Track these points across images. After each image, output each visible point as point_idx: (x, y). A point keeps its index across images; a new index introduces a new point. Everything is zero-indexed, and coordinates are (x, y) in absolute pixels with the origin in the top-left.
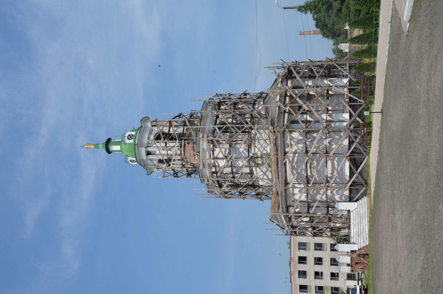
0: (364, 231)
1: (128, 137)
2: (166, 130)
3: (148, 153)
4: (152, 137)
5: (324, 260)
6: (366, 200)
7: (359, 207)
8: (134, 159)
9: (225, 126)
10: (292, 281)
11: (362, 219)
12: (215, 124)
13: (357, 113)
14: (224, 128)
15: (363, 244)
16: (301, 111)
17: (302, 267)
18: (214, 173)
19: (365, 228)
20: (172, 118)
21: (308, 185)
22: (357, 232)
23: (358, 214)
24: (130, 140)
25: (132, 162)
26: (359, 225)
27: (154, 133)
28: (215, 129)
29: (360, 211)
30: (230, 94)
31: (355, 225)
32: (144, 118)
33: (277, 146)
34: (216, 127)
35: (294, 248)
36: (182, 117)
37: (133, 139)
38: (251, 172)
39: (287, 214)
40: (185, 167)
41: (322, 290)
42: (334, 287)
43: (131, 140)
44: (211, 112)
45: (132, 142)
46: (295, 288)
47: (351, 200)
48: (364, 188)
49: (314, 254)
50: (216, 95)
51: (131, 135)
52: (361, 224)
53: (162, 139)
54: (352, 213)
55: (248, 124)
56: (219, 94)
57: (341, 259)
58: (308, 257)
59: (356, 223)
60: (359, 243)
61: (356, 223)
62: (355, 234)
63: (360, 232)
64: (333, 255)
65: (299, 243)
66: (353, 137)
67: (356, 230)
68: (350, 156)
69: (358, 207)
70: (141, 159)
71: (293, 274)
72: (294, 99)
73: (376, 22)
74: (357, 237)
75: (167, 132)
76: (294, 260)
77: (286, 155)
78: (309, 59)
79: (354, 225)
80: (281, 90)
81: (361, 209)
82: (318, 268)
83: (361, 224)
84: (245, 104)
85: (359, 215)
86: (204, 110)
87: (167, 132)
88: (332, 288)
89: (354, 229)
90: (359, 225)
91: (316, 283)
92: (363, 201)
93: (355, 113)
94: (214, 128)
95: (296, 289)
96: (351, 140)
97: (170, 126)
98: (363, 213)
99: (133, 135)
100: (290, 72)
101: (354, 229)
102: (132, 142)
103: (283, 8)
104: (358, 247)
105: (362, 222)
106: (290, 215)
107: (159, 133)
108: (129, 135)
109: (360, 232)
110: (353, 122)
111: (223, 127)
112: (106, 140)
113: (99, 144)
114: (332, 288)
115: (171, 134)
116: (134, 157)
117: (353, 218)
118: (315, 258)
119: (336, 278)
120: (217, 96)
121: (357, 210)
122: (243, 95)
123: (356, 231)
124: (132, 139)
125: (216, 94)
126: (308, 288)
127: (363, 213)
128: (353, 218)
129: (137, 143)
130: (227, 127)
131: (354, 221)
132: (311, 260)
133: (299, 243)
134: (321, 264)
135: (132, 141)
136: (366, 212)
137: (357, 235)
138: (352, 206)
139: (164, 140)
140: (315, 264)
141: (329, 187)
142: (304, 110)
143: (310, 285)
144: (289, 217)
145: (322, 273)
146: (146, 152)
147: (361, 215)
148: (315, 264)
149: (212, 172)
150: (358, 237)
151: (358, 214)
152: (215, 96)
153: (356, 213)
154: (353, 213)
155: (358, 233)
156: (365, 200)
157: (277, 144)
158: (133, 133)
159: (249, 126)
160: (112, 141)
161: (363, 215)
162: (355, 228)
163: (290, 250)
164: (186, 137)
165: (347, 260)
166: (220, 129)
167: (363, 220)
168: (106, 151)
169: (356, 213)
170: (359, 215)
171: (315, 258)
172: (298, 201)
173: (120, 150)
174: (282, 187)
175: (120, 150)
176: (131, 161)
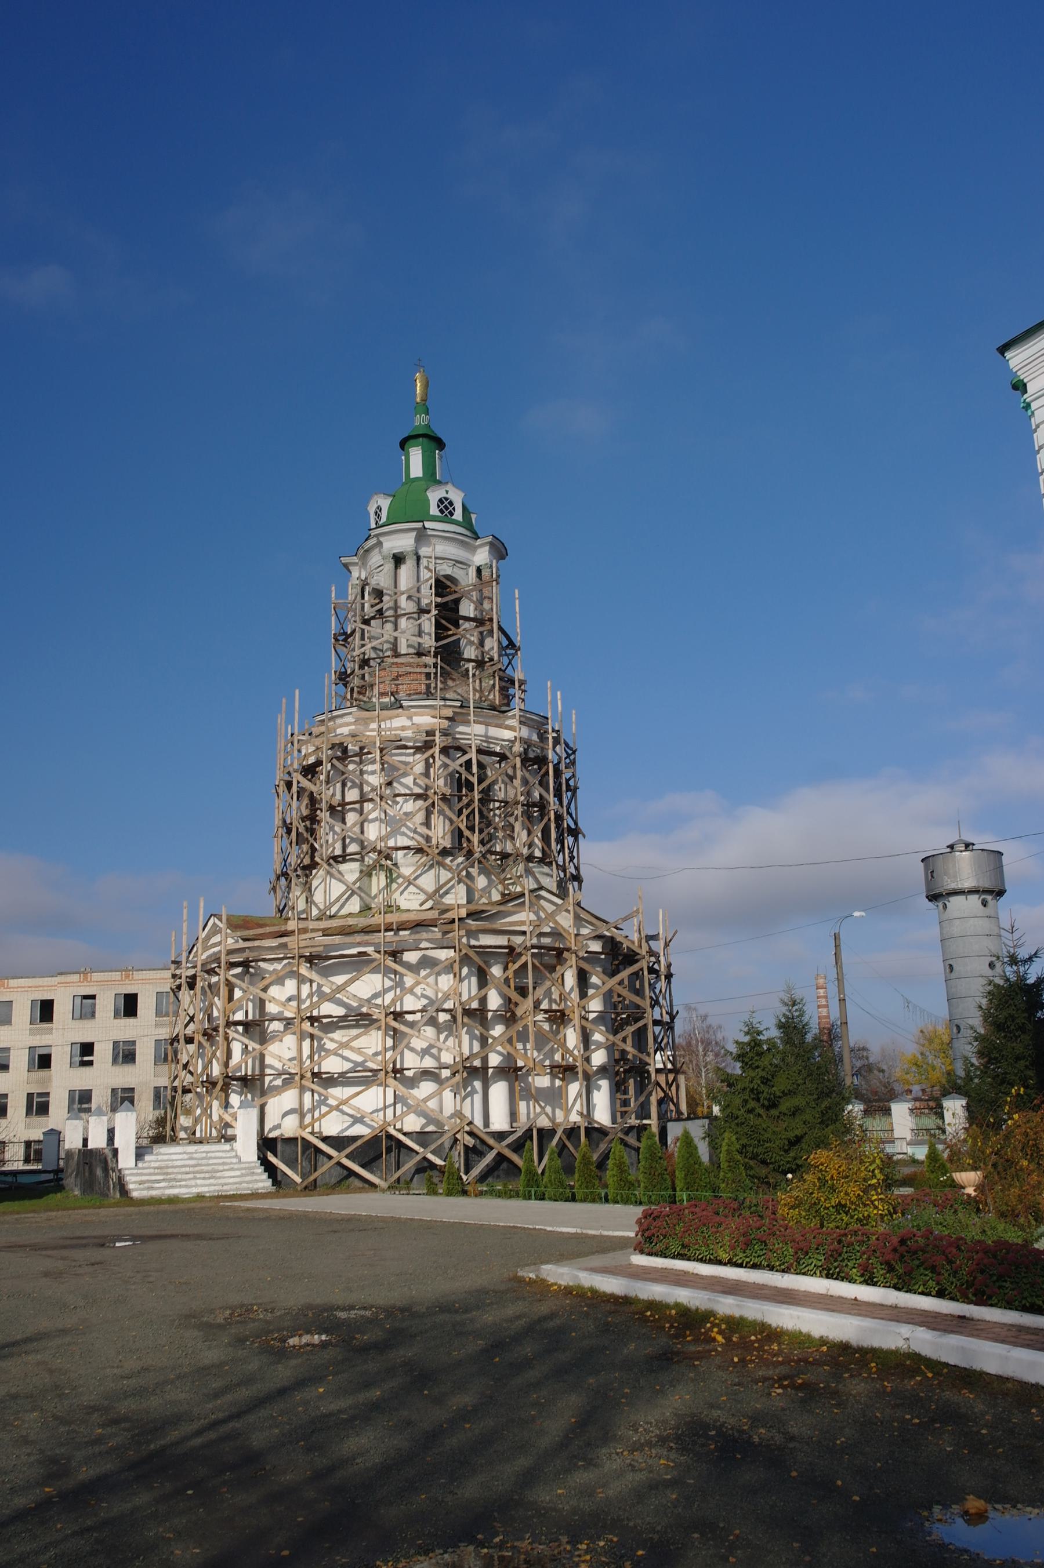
0: (171, 1184)
1: (446, 499)
2: (467, 609)
3: (398, 560)
4: (446, 569)
5: (128, 1068)
6: (261, 1185)
7: (243, 1166)
8: (384, 519)
9: (475, 780)
10: (63, 976)
11: (207, 1175)
12: (480, 751)
13: (508, 1153)
14: (470, 778)
15: (135, 1182)
16: (515, 996)
17: (106, 1005)
18: (345, 750)
19: (180, 1187)
20: (502, 626)
21: (392, 1016)
22: (170, 1164)
23: (224, 1164)
24: (439, 506)
25: (376, 513)
26: (192, 1169)
27: (457, 573)
28: (465, 753)
29: (232, 1169)
30: (576, 788)
31: (191, 1159)
32: (503, 544)
33: (415, 929)
34: (473, 755)
35: (163, 979)
36: (507, 655)
37: (440, 514)
38: (348, 858)
39: (223, 964)
40: (361, 667)
41: (39, 1068)
42: (48, 1101)
43: (437, 510)
44: (515, 737)
45: (431, 513)
46: (43, 986)
47: (267, 1144)
48: (298, 1179)
49: (145, 1039)
50: (571, 749)
51: (454, 509)
52: (194, 1173)
53: (439, 600)
54: (227, 1147)
55: (481, 845)
56: (574, 759)
57: (98, 1120)
58: (135, 1020)
59: (199, 1159)
60: (139, 1171)
61: (199, 1159)
62: (165, 1157)
63: (170, 1170)
64: (100, 1098)
65: (136, 995)
66: (439, 1142)
67: (176, 1160)
68: (389, 1137)
69: (244, 1163)
70: (381, 539)
71: (85, 979)
72: (548, 975)
73: (685, 1198)
74: (157, 1164)
75: (461, 613)
76: (127, 982)
77: (387, 956)
78: (677, 1012)
79: (192, 1153)
80: (573, 936)
81: (238, 1173)
82: (103, 1053)
83: (194, 1173)
84: (359, 1143)
85: (221, 1168)
86: (523, 719)
87: (461, 613)
88: (48, 1094)
89: (180, 1154)
90: (192, 1169)
91: (60, 1048)
92: (134, 1179)
93: (508, 1146)
94: (468, 749)
95: (41, 989)
96: (435, 1136)
97: (479, 622)
98: (224, 1178)
99: (452, 514)
100: (631, 958)
101: (180, 1154)
102: (431, 513)
103: (837, 932)
104: (126, 1169)
105: (198, 1176)
106: (222, 973)
107: (454, 588)
108: (451, 503)
109: (170, 1170)
110: (483, 1142)
111: (473, 775)
112: (439, 435)
113: (427, 413)
114: (48, 1094)
115: (457, 626)
116: (388, 518)
117: (213, 1152)
118: (134, 1043)
119: (76, 1106)
120: (570, 752)
121: (235, 1160)
122: (573, 826)
123: (173, 1160)
124: (441, 511)
125: (576, 750)
126: (45, 1025)
127: (224, 1178)
128: (213, 1152)
129: (426, 526)
130: (473, 784)
131: (204, 1155)
132: (126, 1029)
133: (136, 995)
134: (115, 1061)
135: (434, 511)
136: (225, 1188)
137: (163, 1164)
138: (247, 1148)
139: (436, 606)
140: (116, 1044)
141: (301, 1079)
142: (516, 1004)
143: (54, 1031)
144: (217, 970)
145: (90, 1063)
146: (402, 553)
147: (218, 1174)
148: (116, 1044)
149: (345, 745)
150: (155, 1168)
151: (224, 1164)
152: (567, 745)
153: (225, 1160)
154: (228, 1151)
155: (168, 1167)
156: (264, 1183)
157: (419, 929)
158: (458, 515)
159: (476, 847)
160: (437, 452)
161: (220, 1178)
162: (186, 1156)
163: (161, 967)
164: (445, 666)
165: (97, 1141)
166: (468, 763)
167: (204, 1178)
168: (406, 435)
169: (225, 1160)
170: (221, 1168)
171: (134, 1043)
172: (262, 995)
173: (412, 477)
174: (299, 948)
175: (412, 477)
176: (379, 508)
